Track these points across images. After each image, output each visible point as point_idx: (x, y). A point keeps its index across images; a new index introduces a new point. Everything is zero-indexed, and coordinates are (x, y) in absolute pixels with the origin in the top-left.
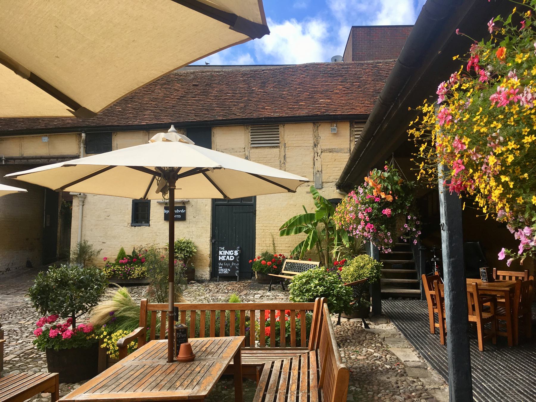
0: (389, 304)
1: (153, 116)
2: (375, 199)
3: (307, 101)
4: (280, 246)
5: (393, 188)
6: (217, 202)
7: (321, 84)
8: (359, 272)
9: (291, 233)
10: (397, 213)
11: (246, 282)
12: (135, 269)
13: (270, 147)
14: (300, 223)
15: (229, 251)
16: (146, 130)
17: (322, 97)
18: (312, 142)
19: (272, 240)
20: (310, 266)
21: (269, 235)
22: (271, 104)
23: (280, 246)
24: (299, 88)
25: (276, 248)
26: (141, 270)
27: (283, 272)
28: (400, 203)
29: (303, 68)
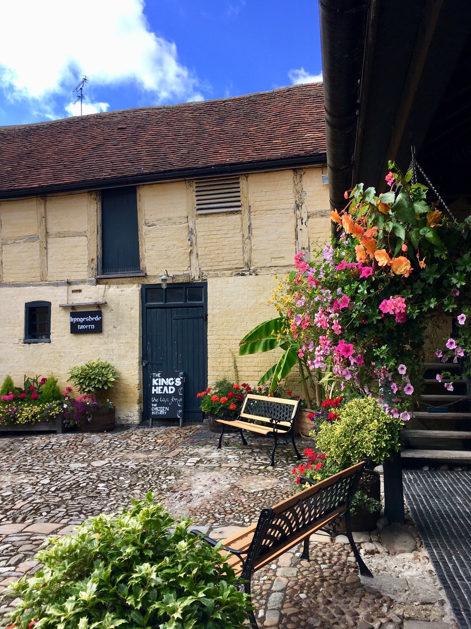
0: (422, 482)
1: (52, 175)
2: (360, 271)
3: (285, 138)
4: (245, 369)
5: (413, 236)
6: (148, 303)
7: (309, 112)
8: (353, 437)
9: (258, 350)
10: (425, 309)
11: (193, 427)
12: (23, 410)
13: (227, 213)
14: (268, 333)
15: (167, 379)
16: (41, 197)
17: (309, 130)
18: (293, 201)
19: (232, 360)
20: (284, 407)
21: (228, 353)
22: (229, 146)
23: (245, 369)
24: (275, 121)
25: (240, 374)
26: (32, 411)
27: (243, 415)
28: (435, 279)
29: (284, 93)
